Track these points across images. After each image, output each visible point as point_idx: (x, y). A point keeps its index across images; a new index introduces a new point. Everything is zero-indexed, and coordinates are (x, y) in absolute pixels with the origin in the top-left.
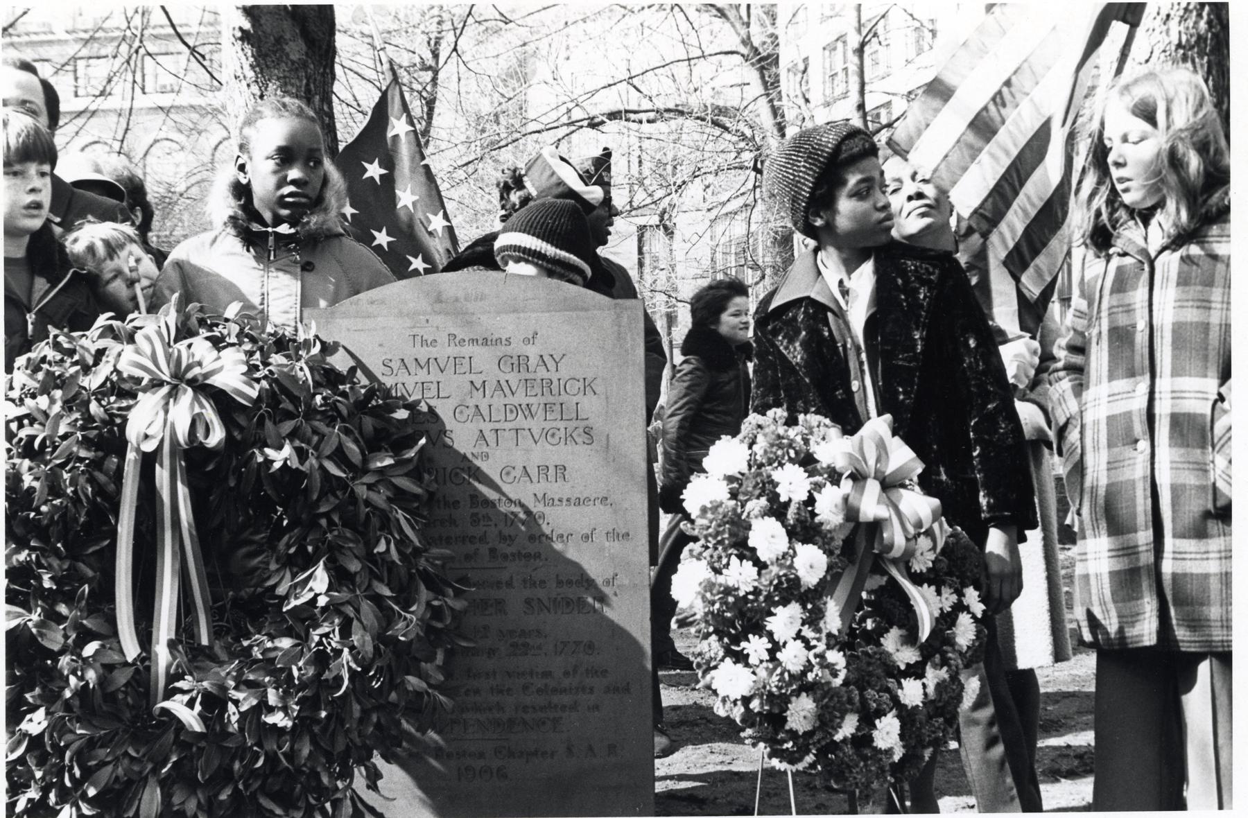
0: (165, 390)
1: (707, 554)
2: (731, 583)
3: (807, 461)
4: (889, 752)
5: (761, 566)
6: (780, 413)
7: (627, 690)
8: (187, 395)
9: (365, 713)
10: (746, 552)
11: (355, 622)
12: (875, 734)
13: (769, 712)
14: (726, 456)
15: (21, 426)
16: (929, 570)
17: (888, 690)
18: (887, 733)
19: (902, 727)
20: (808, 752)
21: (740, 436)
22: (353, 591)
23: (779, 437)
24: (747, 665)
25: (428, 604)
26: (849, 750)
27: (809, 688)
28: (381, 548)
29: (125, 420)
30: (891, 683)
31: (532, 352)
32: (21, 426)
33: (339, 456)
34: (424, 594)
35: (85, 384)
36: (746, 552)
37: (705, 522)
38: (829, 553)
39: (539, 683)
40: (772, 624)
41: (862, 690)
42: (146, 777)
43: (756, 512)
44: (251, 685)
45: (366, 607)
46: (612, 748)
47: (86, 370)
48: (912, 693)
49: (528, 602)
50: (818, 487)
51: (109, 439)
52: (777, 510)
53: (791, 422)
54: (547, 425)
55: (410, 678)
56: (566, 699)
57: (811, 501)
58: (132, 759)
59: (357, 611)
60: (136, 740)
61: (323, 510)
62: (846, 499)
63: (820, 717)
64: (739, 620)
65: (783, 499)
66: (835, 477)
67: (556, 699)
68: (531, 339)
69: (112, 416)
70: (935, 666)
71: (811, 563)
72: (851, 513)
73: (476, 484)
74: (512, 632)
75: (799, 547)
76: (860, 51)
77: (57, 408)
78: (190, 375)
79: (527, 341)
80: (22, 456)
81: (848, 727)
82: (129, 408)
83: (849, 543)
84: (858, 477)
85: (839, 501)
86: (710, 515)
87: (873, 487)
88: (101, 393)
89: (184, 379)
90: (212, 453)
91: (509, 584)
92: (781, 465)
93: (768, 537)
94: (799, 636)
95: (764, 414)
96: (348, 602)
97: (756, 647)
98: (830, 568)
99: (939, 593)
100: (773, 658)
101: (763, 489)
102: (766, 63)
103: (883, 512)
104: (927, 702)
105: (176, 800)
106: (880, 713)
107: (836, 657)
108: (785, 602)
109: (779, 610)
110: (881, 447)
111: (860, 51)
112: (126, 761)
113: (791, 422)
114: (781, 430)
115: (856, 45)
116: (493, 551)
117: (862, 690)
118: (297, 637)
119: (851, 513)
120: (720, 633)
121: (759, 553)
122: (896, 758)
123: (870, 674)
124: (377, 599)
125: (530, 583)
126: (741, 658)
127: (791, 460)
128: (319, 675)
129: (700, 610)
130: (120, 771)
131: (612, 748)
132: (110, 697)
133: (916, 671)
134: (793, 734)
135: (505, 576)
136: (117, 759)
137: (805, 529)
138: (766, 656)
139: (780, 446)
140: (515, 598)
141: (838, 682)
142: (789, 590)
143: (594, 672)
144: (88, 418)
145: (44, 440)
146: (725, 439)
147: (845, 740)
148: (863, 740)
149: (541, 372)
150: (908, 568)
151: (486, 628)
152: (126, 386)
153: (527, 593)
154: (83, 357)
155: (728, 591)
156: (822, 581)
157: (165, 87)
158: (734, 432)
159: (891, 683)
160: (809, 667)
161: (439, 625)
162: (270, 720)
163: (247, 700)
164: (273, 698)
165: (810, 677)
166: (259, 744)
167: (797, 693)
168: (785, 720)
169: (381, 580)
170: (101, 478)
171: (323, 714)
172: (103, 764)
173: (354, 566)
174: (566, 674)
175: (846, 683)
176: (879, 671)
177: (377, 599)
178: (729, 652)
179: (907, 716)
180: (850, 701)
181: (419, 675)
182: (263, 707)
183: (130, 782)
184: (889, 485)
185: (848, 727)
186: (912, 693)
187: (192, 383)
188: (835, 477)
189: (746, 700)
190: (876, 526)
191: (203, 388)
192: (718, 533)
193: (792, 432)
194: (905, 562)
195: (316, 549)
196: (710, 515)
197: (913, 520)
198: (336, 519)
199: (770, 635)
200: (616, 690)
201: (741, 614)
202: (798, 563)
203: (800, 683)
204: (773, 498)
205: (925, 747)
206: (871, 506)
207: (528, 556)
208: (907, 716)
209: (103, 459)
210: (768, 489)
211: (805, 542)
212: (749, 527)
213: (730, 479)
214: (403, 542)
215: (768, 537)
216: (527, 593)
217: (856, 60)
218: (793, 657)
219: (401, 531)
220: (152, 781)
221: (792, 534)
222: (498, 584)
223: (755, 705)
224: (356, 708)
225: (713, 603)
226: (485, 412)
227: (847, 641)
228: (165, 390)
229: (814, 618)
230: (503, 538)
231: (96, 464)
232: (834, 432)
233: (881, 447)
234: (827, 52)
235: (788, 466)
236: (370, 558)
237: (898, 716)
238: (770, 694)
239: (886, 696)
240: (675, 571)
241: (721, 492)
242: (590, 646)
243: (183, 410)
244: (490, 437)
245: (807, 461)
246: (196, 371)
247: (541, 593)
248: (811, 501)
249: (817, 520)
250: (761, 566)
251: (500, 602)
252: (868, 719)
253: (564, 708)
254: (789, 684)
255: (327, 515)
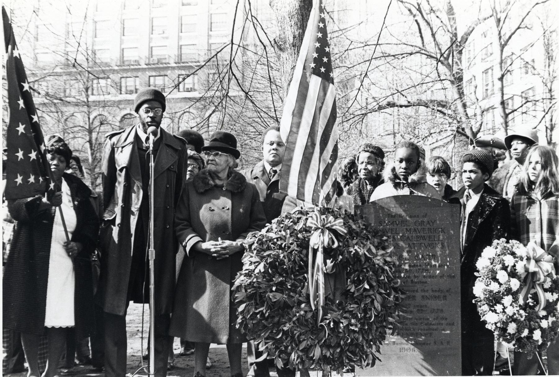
0: (320, 230)
1: (484, 281)
2: (492, 289)
3: (513, 254)
4: (538, 341)
5: (500, 284)
6: (503, 240)
7: (453, 324)
8: (327, 232)
9: (377, 328)
10: (495, 279)
11: (375, 301)
12: (533, 335)
13: (503, 327)
14: (488, 252)
15: (277, 240)
16: (549, 288)
17: (537, 322)
18: (537, 335)
19: (542, 334)
20: (513, 340)
21: (492, 246)
22: (374, 291)
23: (505, 247)
24: (496, 313)
25: (394, 296)
26: (525, 340)
27: (515, 320)
28: (382, 278)
29: (309, 240)
30: (538, 320)
31: (425, 220)
32: (277, 240)
33: (369, 250)
34: (393, 293)
35: (296, 228)
36: (495, 279)
37: (484, 272)
38: (520, 281)
39: (426, 322)
40: (503, 301)
41: (530, 322)
42: (316, 345)
43: (499, 268)
44: (345, 318)
45: (378, 296)
46: (448, 343)
47: (295, 223)
48: (544, 324)
49: (423, 297)
50: (517, 262)
51: (304, 244)
52: (505, 268)
53: (507, 242)
54: (430, 242)
55: (389, 318)
56: (435, 327)
57: (514, 266)
58: (312, 339)
59: (376, 297)
60: (312, 334)
61: (365, 266)
62: (525, 265)
63: (517, 329)
64: (494, 300)
65: (506, 265)
66: (521, 259)
67: (431, 327)
68: (425, 216)
69: (305, 238)
70: (551, 317)
71: (515, 284)
72: (527, 270)
73: (177, 277)
74: (418, 306)
75: (511, 279)
76: (501, 79)
77: (288, 236)
78: (327, 226)
79: (423, 216)
80: (279, 249)
81: (526, 333)
82: (310, 236)
83: (526, 277)
84: (528, 259)
85: (523, 266)
86: (485, 269)
87: (533, 262)
88: (300, 231)
89: (324, 228)
90: (334, 249)
91: (417, 291)
92: (505, 255)
93: (502, 276)
94: (511, 305)
95: (499, 240)
96: (373, 295)
97: (499, 308)
98: (521, 285)
99: (552, 294)
100: (504, 312)
101: (501, 262)
102: (458, 80)
103: (537, 269)
104: (549, 327)
105: (324, 352)
106: (535, 329)
107: (522, 312)
108: (507, 295)
109: (506, 297)
110: (534, 250)
111: (501, 79)
112: (310, 340)
113: (507, 242)
114: (505, 245)
115: (500, 76)
116: (412, 281)
117: (530, 322)
118: (358, 304)
119: (527, 270)
120: (488, 304)
121: (500, 280)
122: (540, 343)
123: (532, 318)
124: (380, 294)
125: (423, 291)
126: (495, 311)
127: (508, 254)
128: (365, 316)
129: (482, 297)
130: (309, 343)
131: (448, 343)
132: (307, 321)
133: (546, 318)
134: (509, 334)
135: (416, 288)
136: (308, 339)
137: (513, 274)
138: (502, 311)
139: (505, 249)
140: (419, 295)
141: (522, 319)
142: (509, 291)
143: (443, 318)
144: (298, 238)
145: (285, 245)
146: (488, 247)
147: (524, 337)
148: (530, 337)
149: (428, 226)
150: (543, 287)
151: (409, 304)
152: (308, 229)
153: (423, 294)
154: (294, 220)
155: (491, 292)
156: (518, 289)
157: (188, 89)
158: (490, 245)
159: (538, 320)
160: (514, 314)
161: (397, 302)
162: (352, 328)
163: (345, 322)
164: (353, 321)
165: (515, 317)
166: (349, 336)
167: (511, 322)
168: (507, 330)
169: (382, 288)
170: (302, 256)
171: (367, 327)
172: (304, 340)
173: (374, 284)
174: (434, 319)
175: (525, 320)
176: (535, 317)
177: (380, 294)
178: (490, 310)
179: (543, 330)
180: (526, 325)
181: (392, 317)
182: (350, 324)
183: (311, 346)
184: (537, 261)
185: (526, 333)
186: (544, 324)
187: (328, 228)
188: (521, 259)
189: (496, 323)
190: (534, 274)
191: (331, 230)
192: (488, 275)
193: (508, 245)
194: (541, 285)
195: (363, 278)
196: (485, 269)
197: (545, 270)
198: (369, 269)
199: (503, 304)
200: (450, 324)
201: (494, 299)
202: (511, 283)
203: (512, 319)
204: (504, 264)
205: (548, 341)
206: (532, 267)
207: (423, 282)
208: (543, 330)
209: (302, 251)
210: (502, 262)
211: (513, 277)
212: (497, 273)
213: (490, 259)
214: (388, 277)
215: (502, 276)
216: (423, 294)
217: (498, 84)
218: (510, 311)
219: (388, 273)
220: (318, 346)
221: (509, 275)
222: (414, 291)
223: (499, 325)
224: (375, 326)
225: (486, 295)
226: (411, 238)
227: (525, 307)
228: (320, 230)
229: (515, 300)
230: (415, 277)
231: (300, 252)
232: (521, 245)
233: (534, 250)
234: (484, 74)
235: (508, 255)
236: (378, 281)
237: (541, 330)
238: (503, 322)
239: (537, 324)
240: (474, 286)
241: (488, 263)
242: (442, 311)
243: (327, 237)
244: (412, 246)
245: (513, 254)
246: (329, 225)
247: (427, 294)
248: (514, 266)
249: (516, 271)
250: (500, 284)
251: (414, 297)
252: (531, 331)
253: (433, 330)
254: (509, 319)
255: (366, 268)
